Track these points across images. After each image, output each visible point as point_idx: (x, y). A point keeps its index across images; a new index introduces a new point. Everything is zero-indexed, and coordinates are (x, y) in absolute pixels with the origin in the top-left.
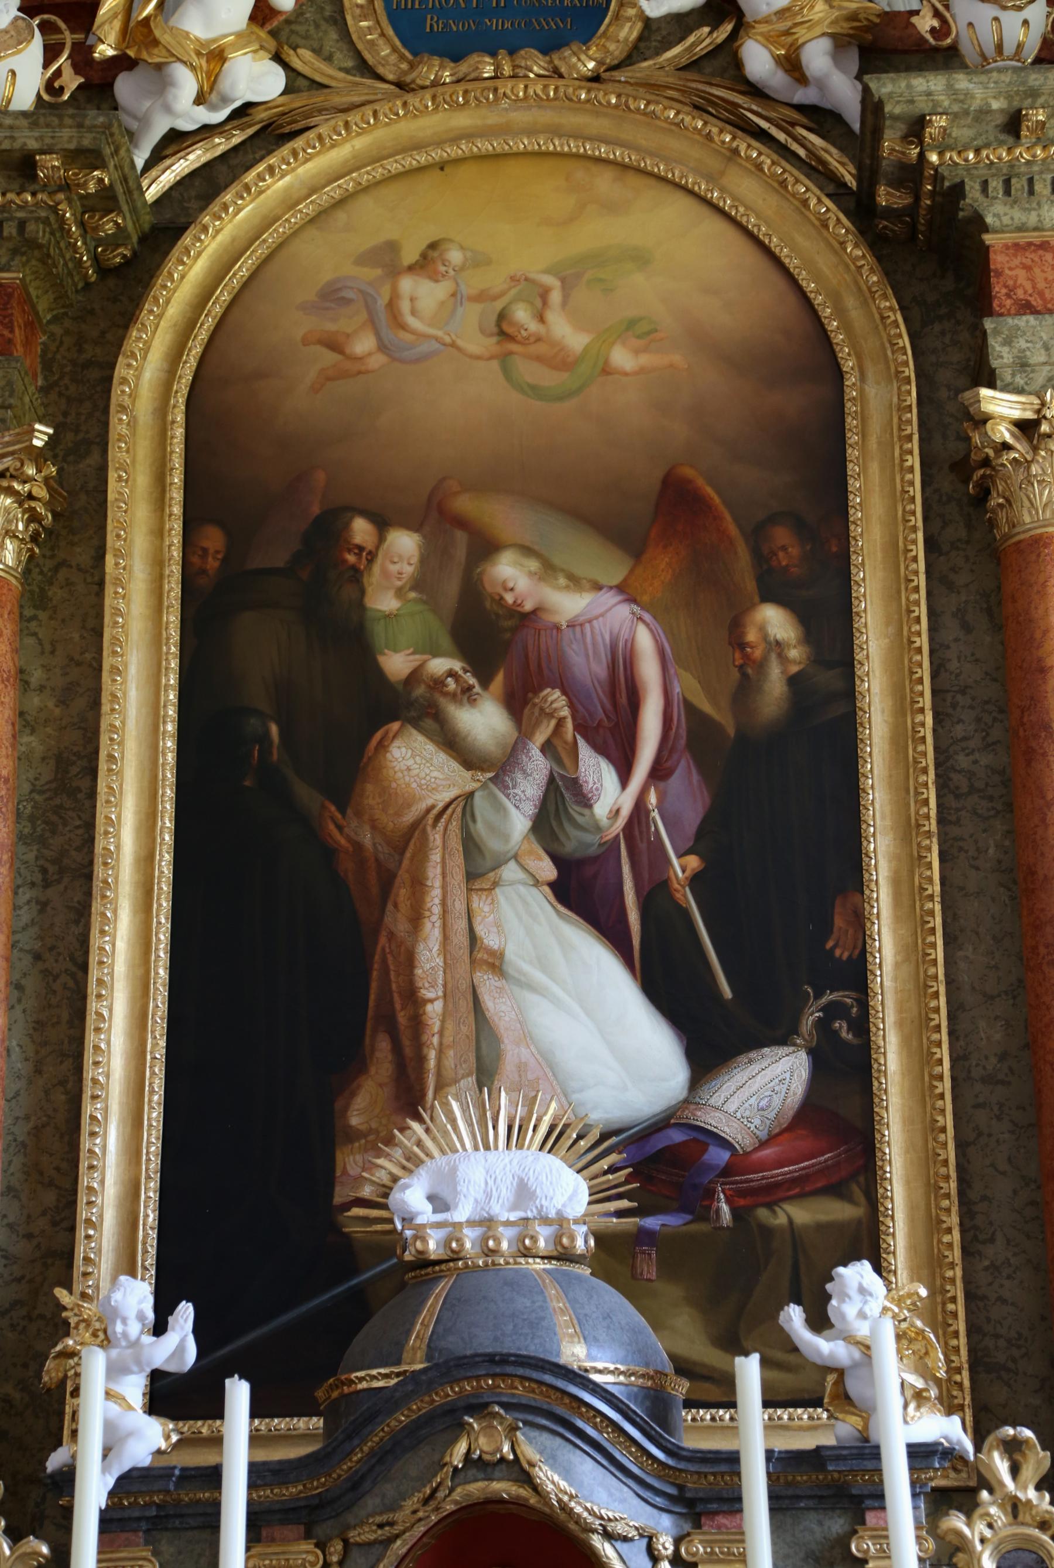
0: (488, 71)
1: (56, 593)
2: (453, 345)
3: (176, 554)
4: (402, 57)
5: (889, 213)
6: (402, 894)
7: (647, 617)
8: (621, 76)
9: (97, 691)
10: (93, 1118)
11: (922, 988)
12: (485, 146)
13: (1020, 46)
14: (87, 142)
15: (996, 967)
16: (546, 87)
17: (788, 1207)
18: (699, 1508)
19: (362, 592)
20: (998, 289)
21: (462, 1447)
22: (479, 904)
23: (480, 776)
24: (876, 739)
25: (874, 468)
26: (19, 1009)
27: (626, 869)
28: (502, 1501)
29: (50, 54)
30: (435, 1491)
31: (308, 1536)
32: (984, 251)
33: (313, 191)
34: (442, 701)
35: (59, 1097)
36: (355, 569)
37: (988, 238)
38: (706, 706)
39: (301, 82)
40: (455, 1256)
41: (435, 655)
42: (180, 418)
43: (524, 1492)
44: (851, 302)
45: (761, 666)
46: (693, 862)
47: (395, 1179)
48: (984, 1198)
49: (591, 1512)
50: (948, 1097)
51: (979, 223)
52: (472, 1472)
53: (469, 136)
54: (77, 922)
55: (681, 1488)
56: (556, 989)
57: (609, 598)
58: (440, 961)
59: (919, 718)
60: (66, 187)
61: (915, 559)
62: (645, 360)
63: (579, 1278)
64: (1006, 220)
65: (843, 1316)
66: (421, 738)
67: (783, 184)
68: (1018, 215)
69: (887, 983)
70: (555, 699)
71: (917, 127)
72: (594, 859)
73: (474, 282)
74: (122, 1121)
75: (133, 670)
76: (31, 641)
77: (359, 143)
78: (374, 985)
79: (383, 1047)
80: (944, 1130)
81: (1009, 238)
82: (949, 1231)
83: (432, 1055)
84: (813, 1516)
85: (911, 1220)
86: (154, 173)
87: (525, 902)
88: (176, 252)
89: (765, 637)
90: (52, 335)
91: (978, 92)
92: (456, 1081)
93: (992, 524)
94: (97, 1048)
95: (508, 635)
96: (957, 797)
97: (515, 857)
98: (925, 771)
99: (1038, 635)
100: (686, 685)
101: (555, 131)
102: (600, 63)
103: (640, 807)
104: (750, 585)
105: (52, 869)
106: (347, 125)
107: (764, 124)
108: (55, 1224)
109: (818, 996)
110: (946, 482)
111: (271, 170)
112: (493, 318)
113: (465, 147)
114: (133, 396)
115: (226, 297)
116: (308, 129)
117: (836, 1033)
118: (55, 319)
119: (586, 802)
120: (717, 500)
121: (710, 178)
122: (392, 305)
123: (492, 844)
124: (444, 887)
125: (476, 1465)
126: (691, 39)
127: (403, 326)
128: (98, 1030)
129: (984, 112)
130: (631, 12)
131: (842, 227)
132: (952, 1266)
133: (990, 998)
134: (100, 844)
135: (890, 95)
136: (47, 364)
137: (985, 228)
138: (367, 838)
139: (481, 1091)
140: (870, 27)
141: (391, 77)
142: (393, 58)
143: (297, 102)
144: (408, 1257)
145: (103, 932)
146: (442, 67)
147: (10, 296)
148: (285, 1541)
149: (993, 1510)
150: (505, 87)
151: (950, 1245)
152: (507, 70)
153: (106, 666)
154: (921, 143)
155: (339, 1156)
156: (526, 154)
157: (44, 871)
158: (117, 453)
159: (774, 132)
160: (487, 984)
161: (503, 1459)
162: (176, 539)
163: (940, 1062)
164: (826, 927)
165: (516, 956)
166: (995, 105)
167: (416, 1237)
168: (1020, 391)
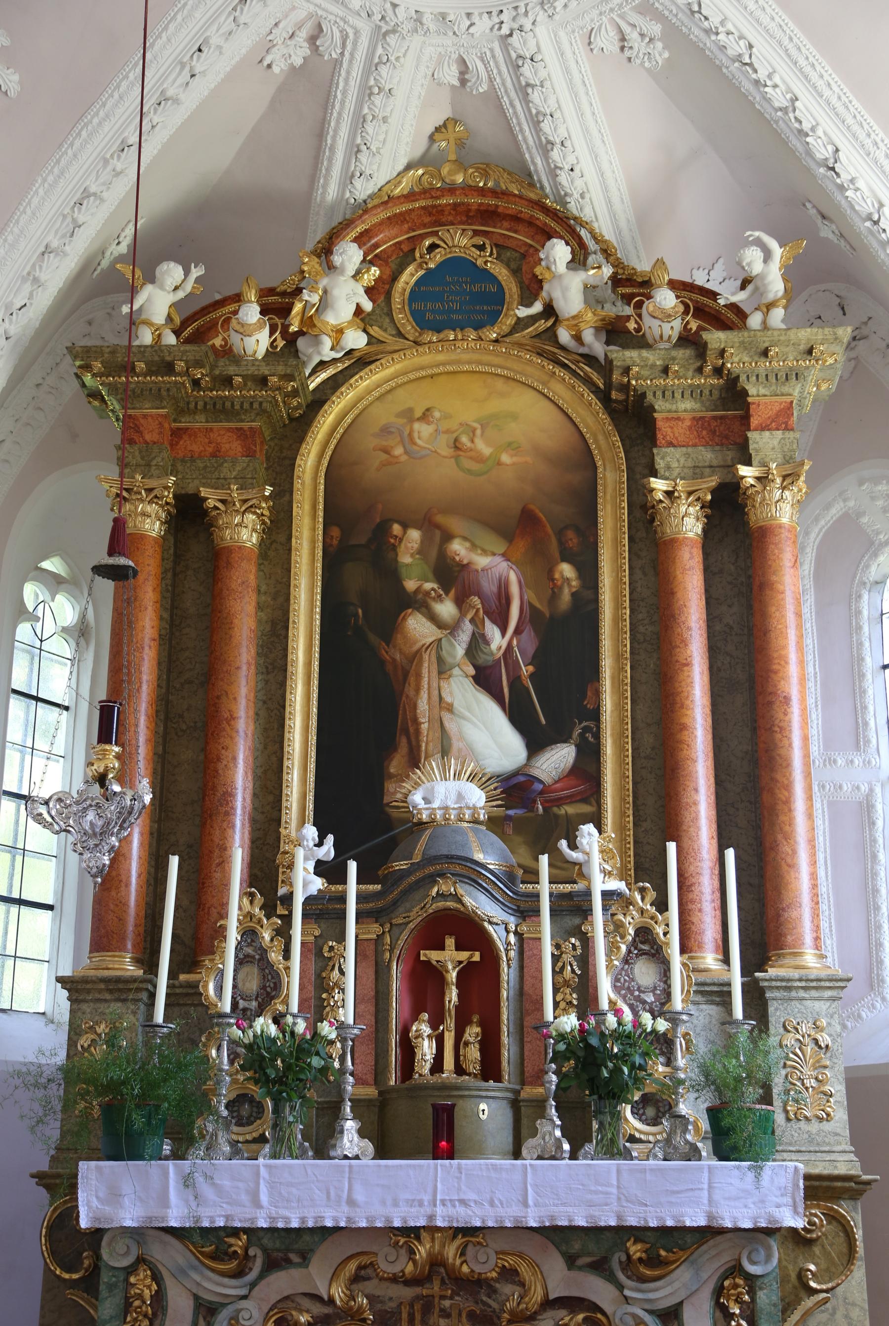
0: (452, 337)
1: (271, 553)
2: (435, 452)
3: (321, 538)
4: (416, 330)
5: (616, 401)
6: (412, 679)
7: (514, 567)
8: (507, 340)
9: (289, 594)
10: (288, 767)
11: (622, 721)
12: (450, 368)
13: (670, 337)
14: (288, 372)
15: (652, 713)
16: (476, 344)
17: (566, 807)
18: (525, 914)
19: (397, 555)
20: (659, 436)
21: (435, 889)
22: (444, 684)
23: (444, 632)
24: (606, 619)
25: (609, 507)
26: (257, 723)
27: (503, 671)
28: (451, 909)
29: (272, 333)
30: (425, 905)
31: (376, 922)
32: (654, 420)
33: (378, 386)
34: (429, 600)
35: (274, 759)
36: (394, 545)
37: (656, 415)
38: (537, 605)
39: (374, 340)
40: (433, 821)
41: (427, 581)
42: (322, 481)
43: (459, 906)
44: (601, 437)
45: (561, 588)
46: (531, 668)
47: (410, 792)
48: (643, 804)
49: (484, 914)
50: (630, 764)
51: (652, 409)
52: (439, 898)
53: (444, 364)
54: (280, 689)
55: (518, 907)
56: (474, 719)
57: (498, 559)
58: (427, 707)
59: (624, 611)
60: (279, 389)
61: (624, 545)
62: (515, 459)
63: (481, 830)
64: (663, 408)
65: (582, 844)
66: (420, 616)
67: (574, 387)
68: (668, 406)
69: (608, 719)
70: (476, 600)
71: (627, 370)
72: (490, 667)
73: (444, 426)
74: (299, 768)
75: (303, 586)
76: (261, 573)
77: (398, 367)
78: (400, 716)
79: (403, 742)
80: (628, 777)
81: (665, 415)
82: (629, 816)
83: (424, 745)
84: (568, 917)
85: (614, 812)
86: (312, 378)
87: (462, 684)
88: (321, 412)
89: (562, 576)
90: (270, 446)
91: (651, 357)
92: (433, 755)
93: (655, 532)
94: (289, 739)
95: (456, 574)
96: (639, 643)
97: (458, 665)
98: (626, 633)
99: (671, 579)
100: (530, 595)
101: (480, 363)
102: (498, 334)
103: (509, 645)
104: (557, 555)
105: (270, 667)
106: (393, 359)
107: (566, 362)
108: (273, 808)
109: (580, 723)
110: (638, 513)
111: (361, 378)
112: (453, 440)
114: (303, 472)
115: (342, 431)
116: (377, 360)
117: (587, 738)
118: (271, 439)
119: (487, 643)
120: (544, 519)
121: (544, 384)
122: (410, 435)
123: (449, 660)
124: (429, 677)
125: (441, 896)
126: (537, 325)
127: (415, 444)
128: (289, 732)
129: (653, 366)
130: (512, 313)
131: (598, 405)
132: (629, 830)
133: (649, 725)
134: (290, 657)
135: (616, 358)
136: (268, 459)
137: (655, 411)
138: (398, 657)
139: (443, 758)
140: (611, 323)
141: (411, 339)
142: (412, 331)
143: (373, 349)
144: (415, 821)
145: (291, 693)
146: (433, 335)
147: (255, 432)
148: (368, 923)
149: (634, 913)
150: (459, 344)
151: (629, 822)
152: (460, 337)
153: (292, 585)
154: (628, 376)
155: (386, 784)
156: (467, 372)
157: (267, 668)
158: (297, 496)
159: (570, 365)
160: (446, 716)
161: (451, 894)
162: (320, 532)
163: (628, 750)
164: (584, 696)
165: (459, 705)
166: (658, 363)
167: (418, 813)
168: (666, 479)
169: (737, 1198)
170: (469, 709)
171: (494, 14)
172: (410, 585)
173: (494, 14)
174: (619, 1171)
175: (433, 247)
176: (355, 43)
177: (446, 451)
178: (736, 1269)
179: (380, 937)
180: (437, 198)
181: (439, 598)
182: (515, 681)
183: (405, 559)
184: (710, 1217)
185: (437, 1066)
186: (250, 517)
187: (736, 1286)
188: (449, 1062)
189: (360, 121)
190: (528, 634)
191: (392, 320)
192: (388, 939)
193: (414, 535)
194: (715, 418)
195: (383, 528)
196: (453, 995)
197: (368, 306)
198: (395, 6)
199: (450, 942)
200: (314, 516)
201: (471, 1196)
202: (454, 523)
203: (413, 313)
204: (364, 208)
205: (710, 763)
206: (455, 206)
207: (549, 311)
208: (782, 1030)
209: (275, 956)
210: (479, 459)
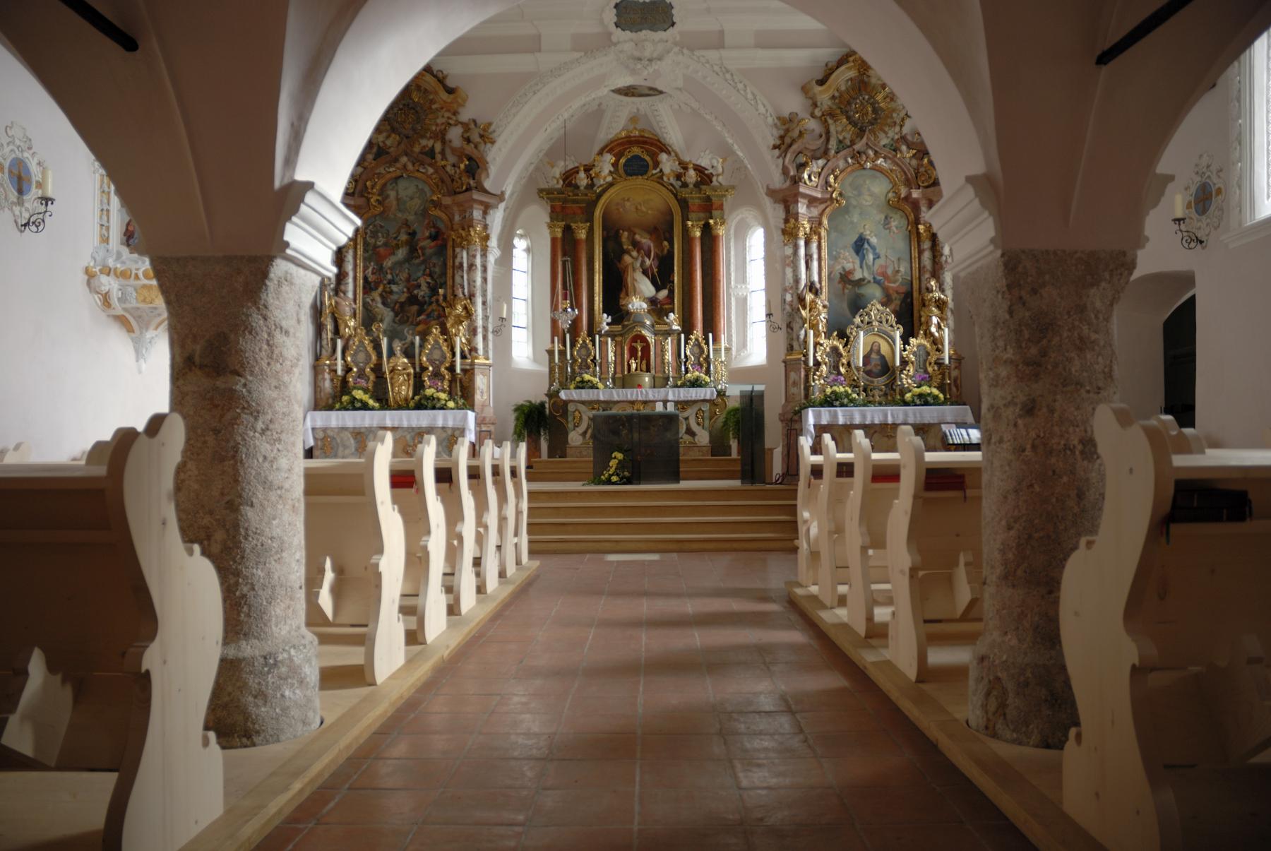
70: (642, 251)
79: (624, 290)
100: (657, 250)
103: (651, 264)
172: (625, 247)
178: (700, 409)
182: (653, 274)
185: (636, 370)
186: (583, 231)
188: (639, 369)
190: (656, 260)
193: (626, 233)
194: (705, 205)
195: (617, 232)
196: (640, 354)
197: (612, 169)
199: (639, 341)
200: (599, 228)
202: (636, 230)
203: (625, 171)
207: (661, 171)
209: (590, 346)
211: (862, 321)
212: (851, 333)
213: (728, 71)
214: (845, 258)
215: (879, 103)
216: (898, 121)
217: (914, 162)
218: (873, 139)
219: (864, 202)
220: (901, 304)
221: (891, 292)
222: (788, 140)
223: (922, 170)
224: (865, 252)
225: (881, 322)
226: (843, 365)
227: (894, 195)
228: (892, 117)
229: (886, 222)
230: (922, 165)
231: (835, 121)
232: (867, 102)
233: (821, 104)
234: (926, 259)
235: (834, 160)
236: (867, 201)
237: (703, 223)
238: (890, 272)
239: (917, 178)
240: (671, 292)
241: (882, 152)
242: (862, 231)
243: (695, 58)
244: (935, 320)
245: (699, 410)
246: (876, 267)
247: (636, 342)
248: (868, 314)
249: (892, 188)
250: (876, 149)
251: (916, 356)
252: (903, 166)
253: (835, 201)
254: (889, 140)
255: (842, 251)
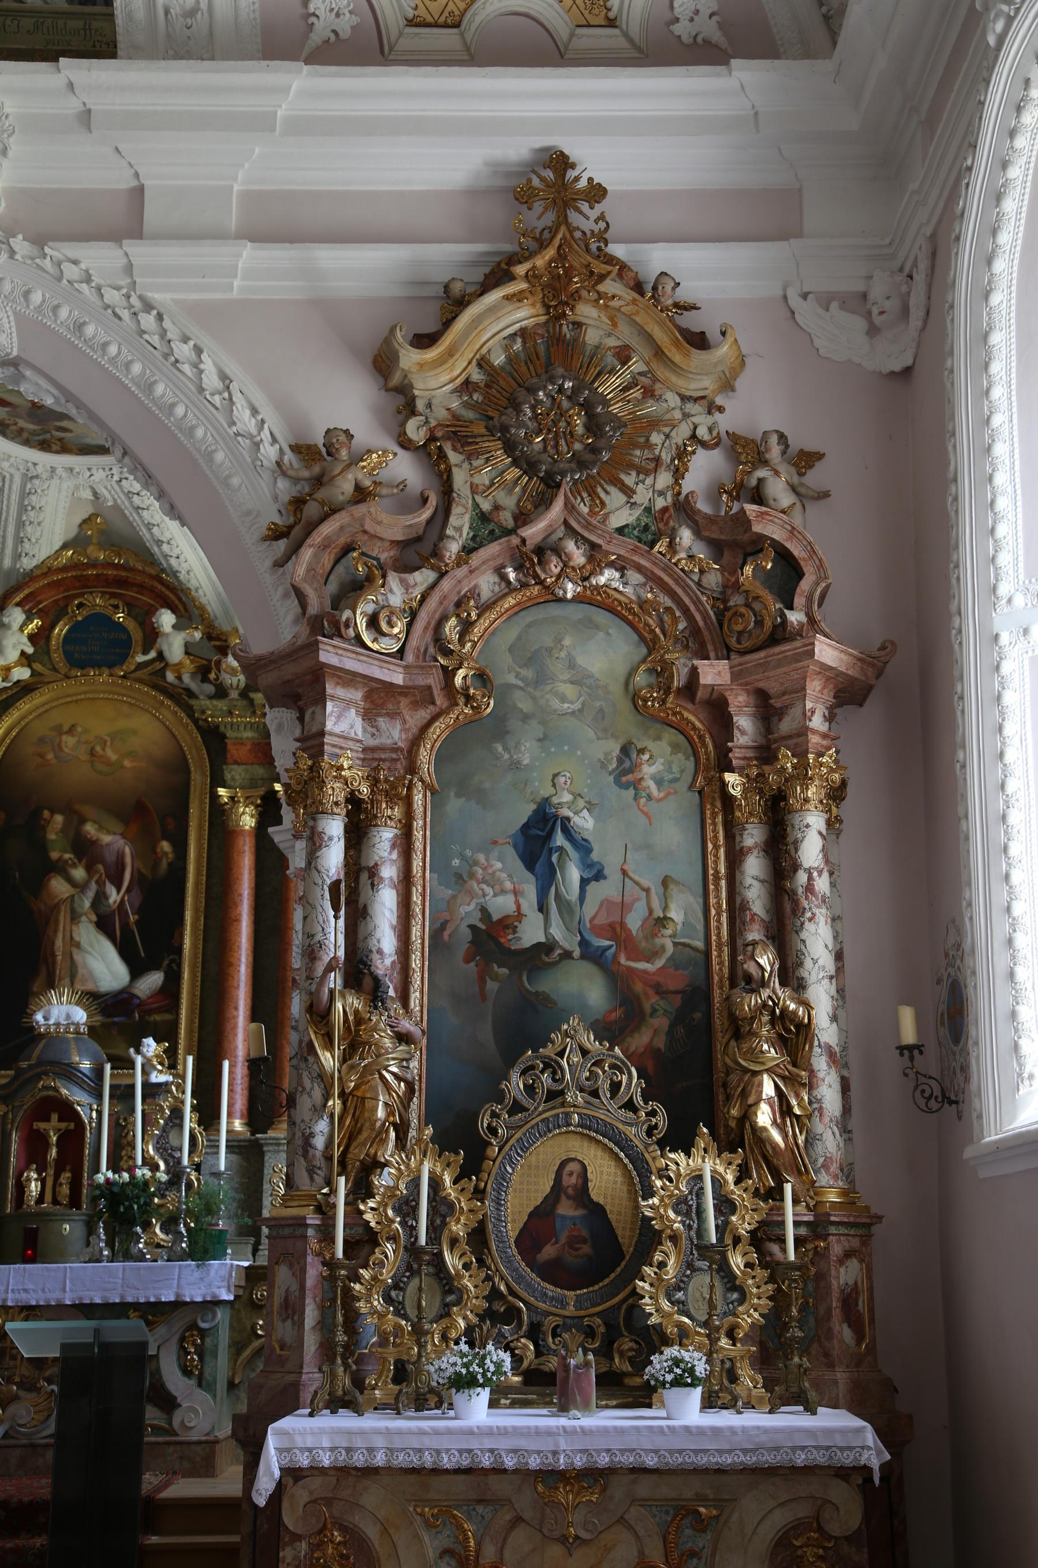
12: (91, 696)
19: (45, 833)
20: (229, 756)
22: (74, 928)
38: (143, 871)
46: (136, 917)
53: (85, 693)
57: (118, 837)
70: (100, 867)
71: (203, 712)
79: (44, 969)
85: (186, 1020)
101: (110, 692)
103: (122, 900)
113: (83, 696)
119: (107, 898)
121: (157, 711)
123: (79, 910)
125: (46, 1088)
143: (35, 679)
150: (96, 678)
156: (102, 698)
160: (75, 951)
165: (84, 942)
169: (195, 1284)
170: (92, 946)
171: (107, 469)
172: (54, 855)
173: (107, 469)
174: (124, 1270)
175: (80, 606)
176: (11, 481)
177: (84, 757)
178: (194, 1326)
179: (6, 1114)
180: (84, 570)
181: (74, 866)
183: (52, 836)
184: (178, 1295)
185: (40, 1199)
187: (193, 1336)
189: (20, 525)
190: (136, 892)
191: (50, 658)
192: (10, 1116)
193: (59, 818)
195: (36, 814)
197: (30, 650)
198: (35, 464)
199: (55, 1117)
201: (31, 1286)
202: (88, 811)
203: (65, 653)
204: (30, 576)
205: (249, 988)
206: (97, 575)
207: (161, 656)
208: (271, 1171)
210: (109, 763)
211: (530, 1090)
212: (493, 1131)
213: (148, 307)
214: (491, 881)
215: (606, 403)
216: (666, 457)
217: (713, 579)
218: (585, 510)
219: (556, 704)
220: (672, 1026)
221: (639, 987)
222: (312, 509)
223: (736, 600)
224: (554, 858)
225: (595, 1094)
226: (454, 1242)
227: (653, 680)
228: (648, 445)
229: (627, 764)
230: (736, 586)
231: (469, 458)
232: (569, 398)
233: (429, 405)
234: (749, 881)
235: (462, 571)
236: (563, 699)
237: (262, 791)
238: (634, 922)
239: (721, 625)
240: (173, 979)
241: (611, 548)
242: (546, 791)
243: (47, 264)
244: (768, 1088)
245: (187, 1330)
246: (590, 909)
247: (48, 1120)
248: (551, 1066)
249: (644, 661)
250: (593, 538)
251: (687, 1214)
252: (679, 591)
253: (461, 701)
254: (638, 512)
255: (481, 858)
